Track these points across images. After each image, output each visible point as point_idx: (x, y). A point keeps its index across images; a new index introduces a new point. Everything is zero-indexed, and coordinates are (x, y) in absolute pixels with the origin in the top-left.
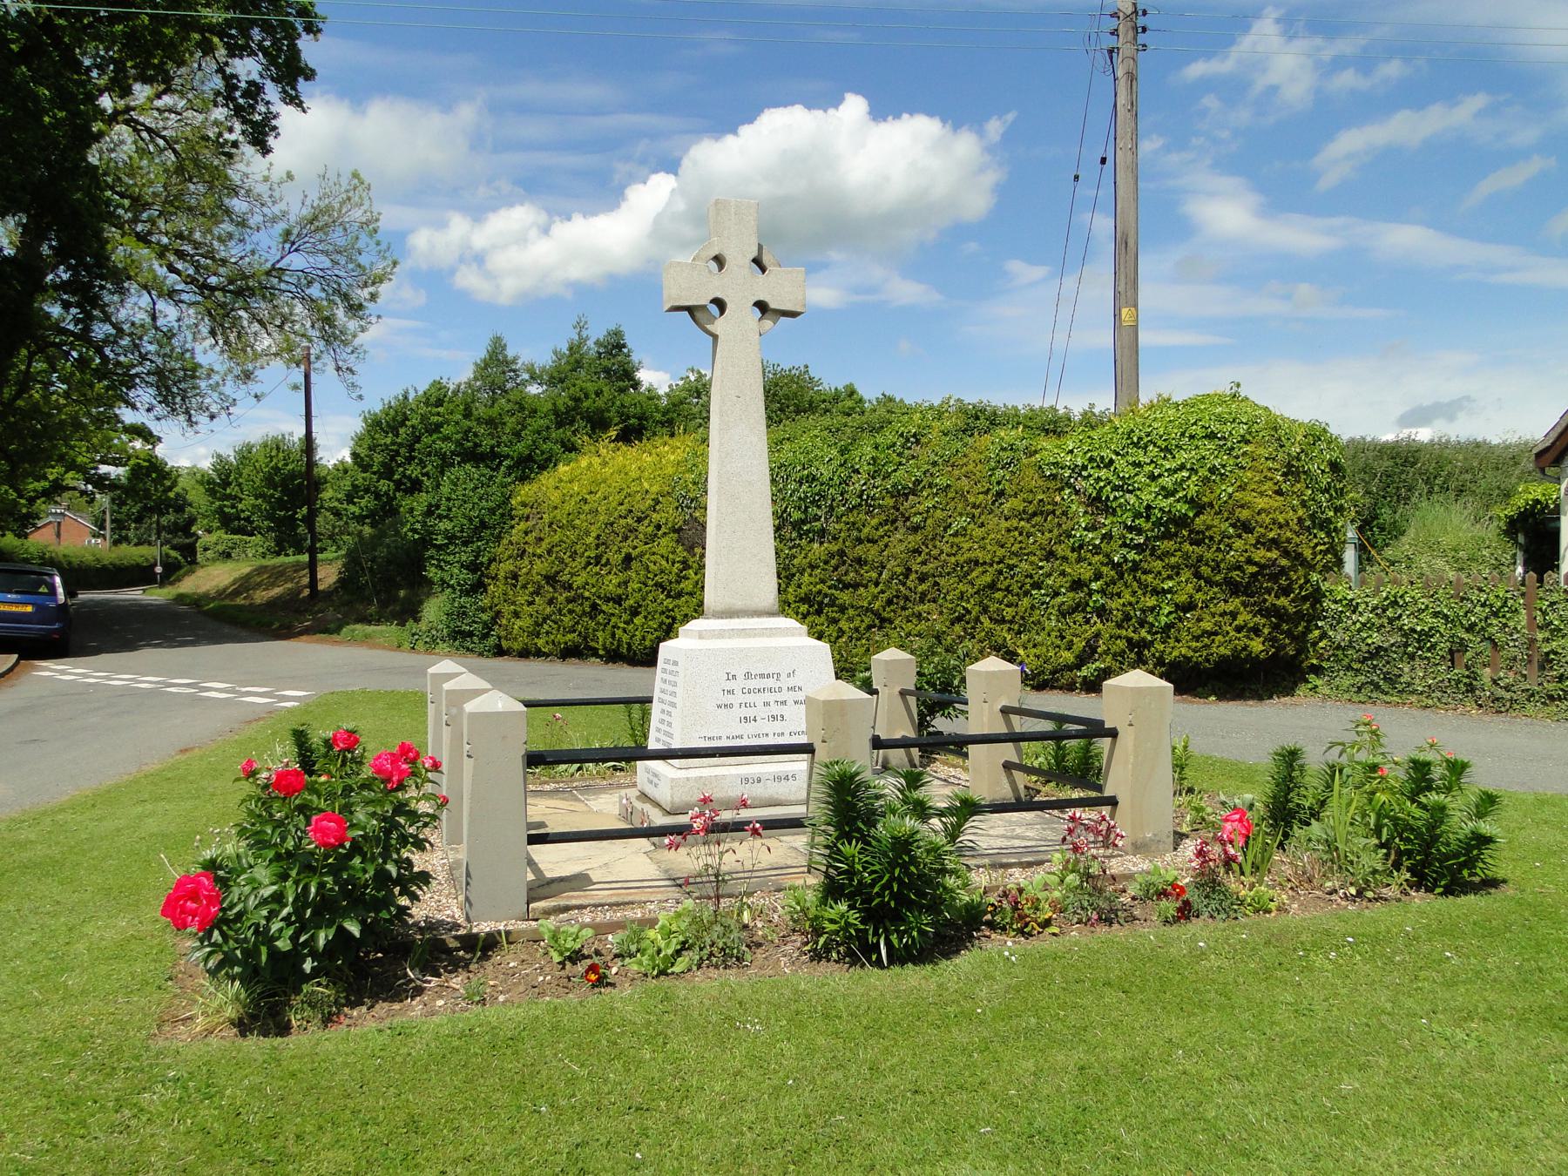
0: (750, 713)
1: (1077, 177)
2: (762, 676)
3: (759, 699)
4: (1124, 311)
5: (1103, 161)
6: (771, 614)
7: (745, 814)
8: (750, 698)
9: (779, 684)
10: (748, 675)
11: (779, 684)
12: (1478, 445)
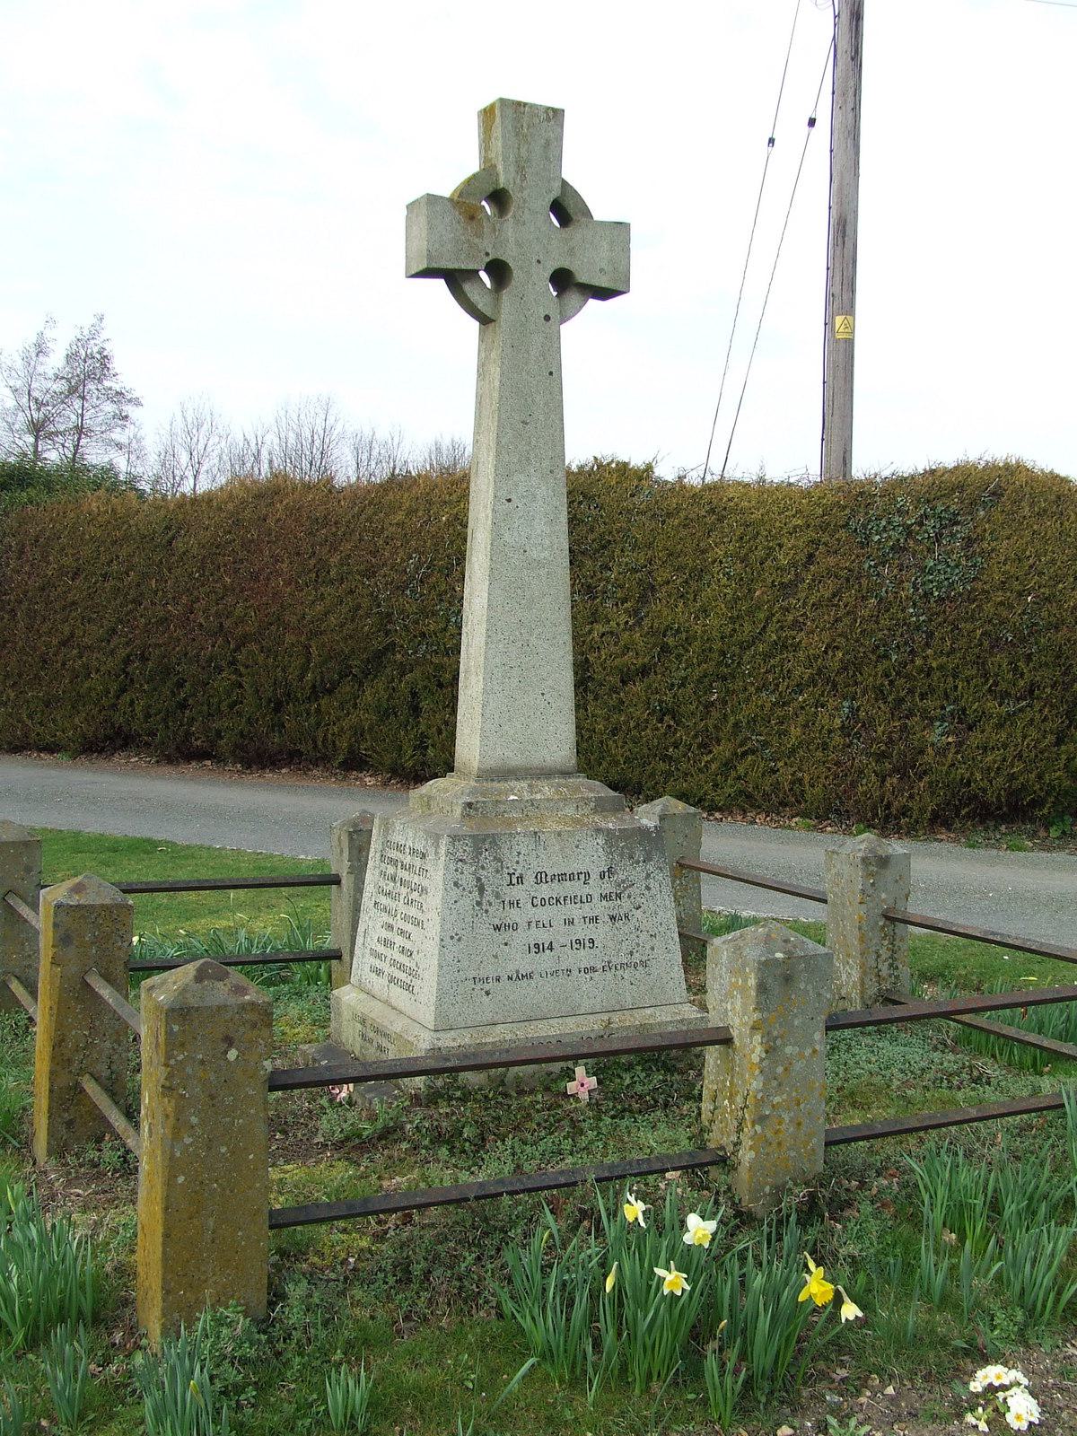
0: (543, 936)
1: (772, 141)
2: (562, 877)
3: (556, 913)
4: (839, 320)
5: (812, 122)
6: (565, 774)
7: (666, 1363)
8: (543, 914)
9: (586, 890)
10: (541, 878)
11: (586, 890)
12: (933, 472)
